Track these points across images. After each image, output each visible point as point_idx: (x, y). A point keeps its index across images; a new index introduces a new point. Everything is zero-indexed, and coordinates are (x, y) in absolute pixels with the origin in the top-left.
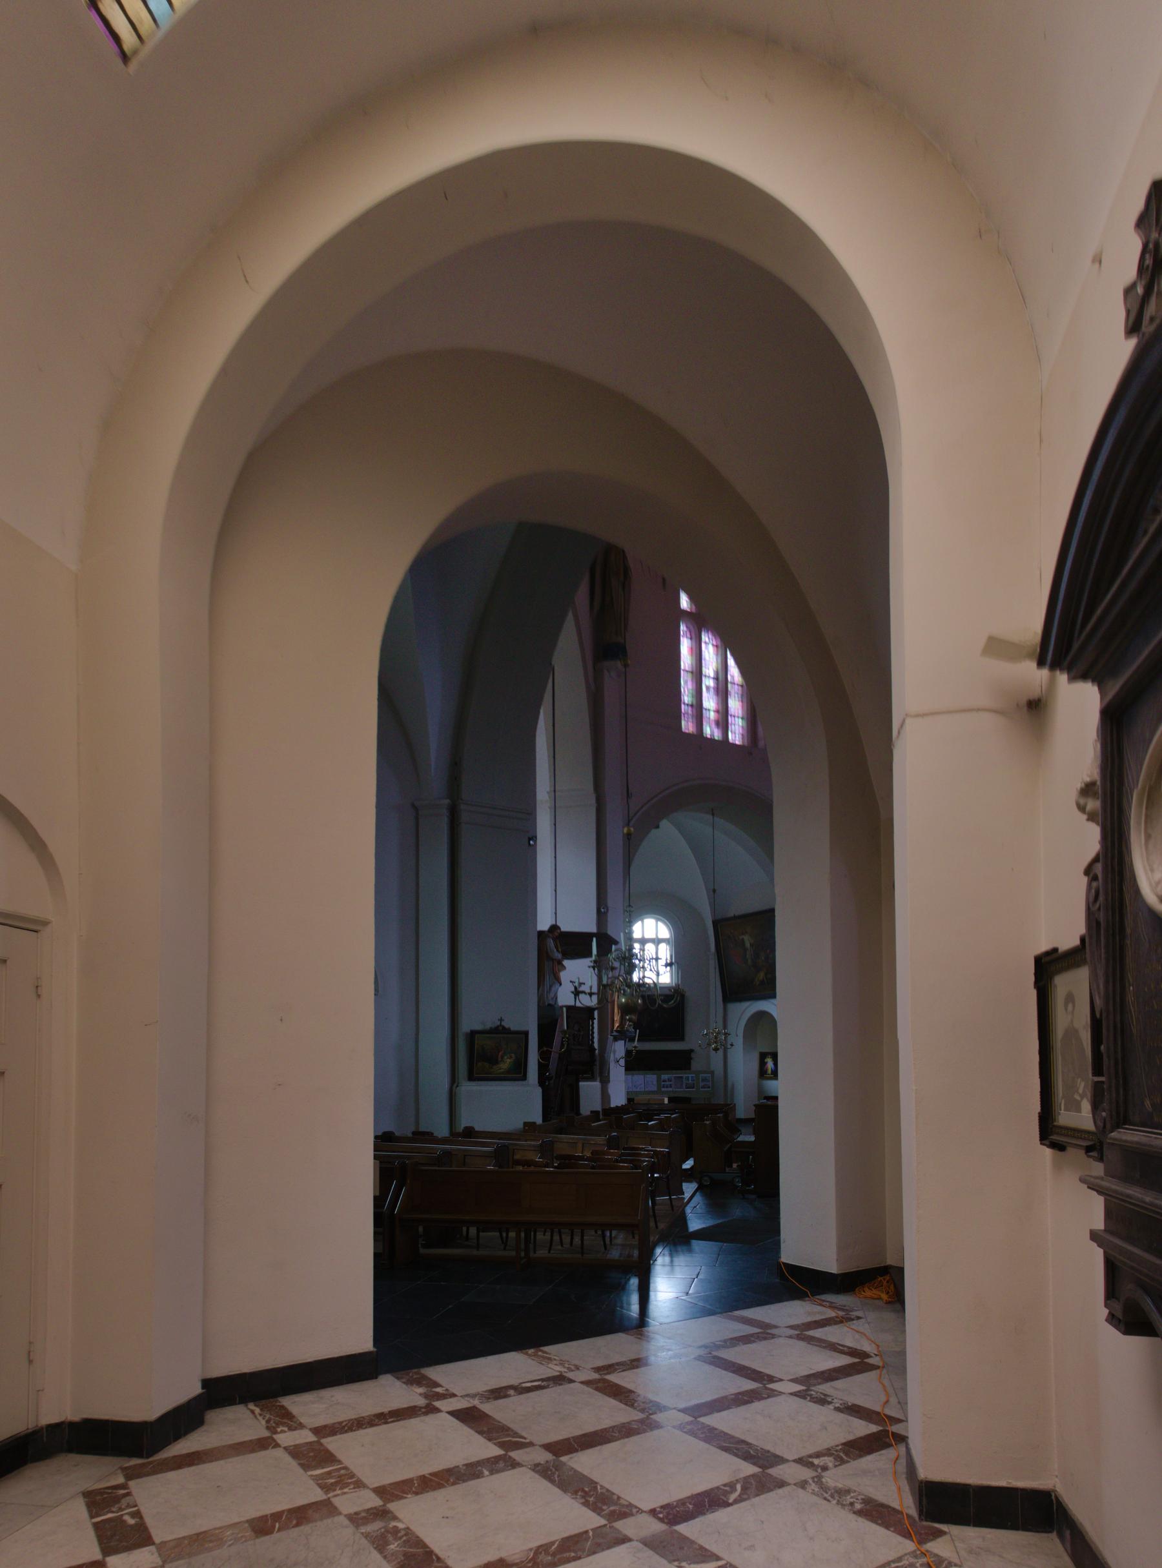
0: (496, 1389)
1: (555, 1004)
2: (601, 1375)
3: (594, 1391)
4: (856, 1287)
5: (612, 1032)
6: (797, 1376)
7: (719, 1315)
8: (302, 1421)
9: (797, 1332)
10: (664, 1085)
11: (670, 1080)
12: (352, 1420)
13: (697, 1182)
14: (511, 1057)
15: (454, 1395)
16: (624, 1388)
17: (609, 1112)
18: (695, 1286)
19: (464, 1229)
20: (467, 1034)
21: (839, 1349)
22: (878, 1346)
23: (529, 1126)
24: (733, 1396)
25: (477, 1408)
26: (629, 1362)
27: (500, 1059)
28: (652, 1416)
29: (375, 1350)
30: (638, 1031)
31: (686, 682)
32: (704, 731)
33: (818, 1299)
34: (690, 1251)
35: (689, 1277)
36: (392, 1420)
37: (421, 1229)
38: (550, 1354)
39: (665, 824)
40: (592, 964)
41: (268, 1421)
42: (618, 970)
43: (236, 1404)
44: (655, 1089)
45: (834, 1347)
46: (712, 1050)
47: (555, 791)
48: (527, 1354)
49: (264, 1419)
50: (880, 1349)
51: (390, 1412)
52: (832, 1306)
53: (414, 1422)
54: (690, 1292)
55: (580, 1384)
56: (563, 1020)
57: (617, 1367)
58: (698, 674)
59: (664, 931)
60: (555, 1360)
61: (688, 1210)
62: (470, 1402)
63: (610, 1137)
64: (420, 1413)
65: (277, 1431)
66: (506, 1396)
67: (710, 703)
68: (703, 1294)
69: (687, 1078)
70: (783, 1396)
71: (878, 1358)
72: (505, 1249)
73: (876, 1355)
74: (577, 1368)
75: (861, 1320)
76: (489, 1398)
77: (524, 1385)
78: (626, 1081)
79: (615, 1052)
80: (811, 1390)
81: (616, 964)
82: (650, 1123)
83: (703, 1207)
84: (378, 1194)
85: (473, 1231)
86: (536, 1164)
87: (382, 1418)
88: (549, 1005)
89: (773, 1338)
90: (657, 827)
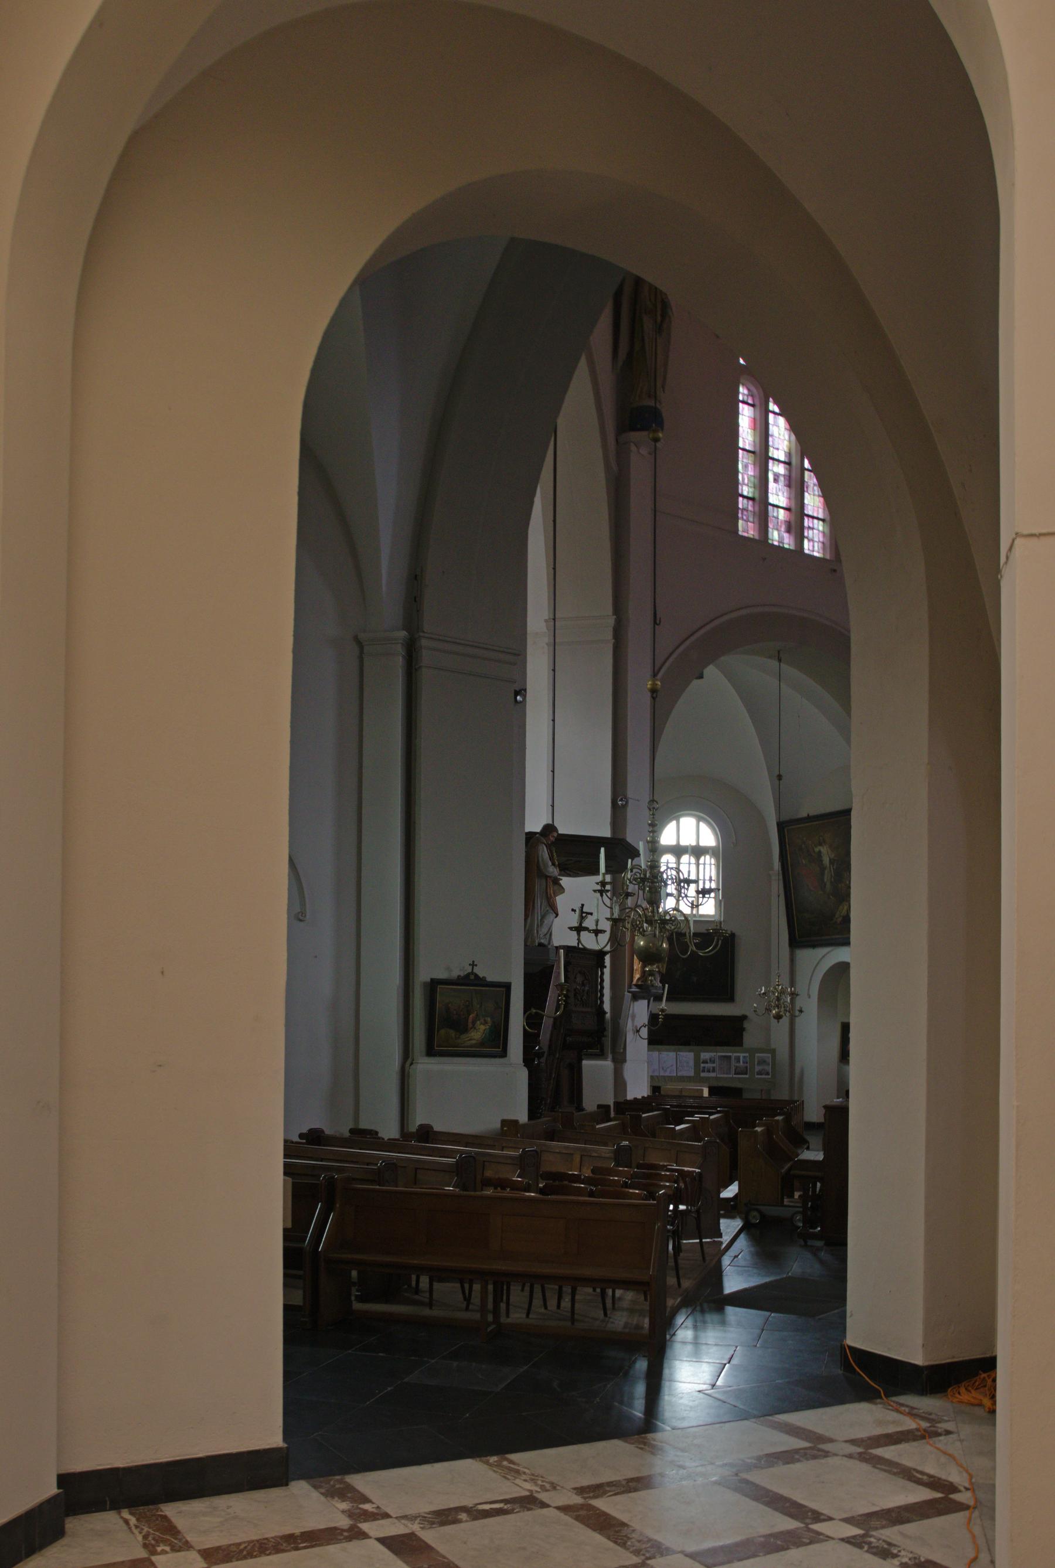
0: (444, 1510)
1: (549, 943)
2: (585, 1498)
3: (574, 1521)
4: (949, 1387)
5: (630, 987)
6: (855, 1514)
7: (754, 1420)
8: (189, 1539)
9: (860, 1450)
10: (704, 1067)
11: (712, 1061)
12: (252, 1541)
13: (741, 1218)
14: (486, 1023)
15: (386, 1516)
16: (615, 1518)
17: (625, 1107)
18: (725, 1375)
19: (414, 1277)
20: (425, 984)
21: (915, 1476)
22: (971, 1476)
23: (510, 1126)
24: (762, 1539)
25: (416, 1536)
26: (624, 1483)
27: (470, 1025)
28: (649, 1562)
29: (286, 1445)
30: (667, 985)
31: (746, 466)
32: (770, 536)
33: (894, 1402)
34: (723, 1323)
35: (718, 1361)
36: (304, 1545)
37: (354, 1274)
38: (518, 1465)
39: (710, 671)
40: (599, 887)
41: (145, 1537)
42: (636, 896)
43: (105, 1510)
44: (692, 1074)
45: (909, 1475)
46: (772, 1018)
47: (554, 619)
48: (487, 1463)
49: (140, 1533)
50: (973, 1480)
51: (303, 1534)
52: (913, 1414)
53: (332, 1549)
54: (719, 1383)
55: (556, 1511)
56: (559, 967)
57: (608, 1489)
58: (762, 456)
59: (708, 838)
60: (524, 1473)
61: (726, 1260)
62: (901, 1533)
63: (620, 1148)
64: (342, 1537)
65: (156, 1551)
66: (456, 1521)
67: (778, 496)
68: (735, 1388)
69: (738, 1059)
70: (831, 1542)
71: (969, 1494)
72: (467, 1309)
73: (967, 1489)
74: (554, 1487)
75: (951, 1436)
76: (433, 1523)
77: (480, 1507)
78: (650, 1063)
79: (634, 1017)
80: (871, 1536)
81: (632, 888)
82: (678, 1128)
83: (748, 1257)
84: (289, 1225)
85: (424, 1281)
86: (515, 1187)
87: (292, 1542)
88: (541, 945)
89: (826, 1456)
90: (701, 677)
